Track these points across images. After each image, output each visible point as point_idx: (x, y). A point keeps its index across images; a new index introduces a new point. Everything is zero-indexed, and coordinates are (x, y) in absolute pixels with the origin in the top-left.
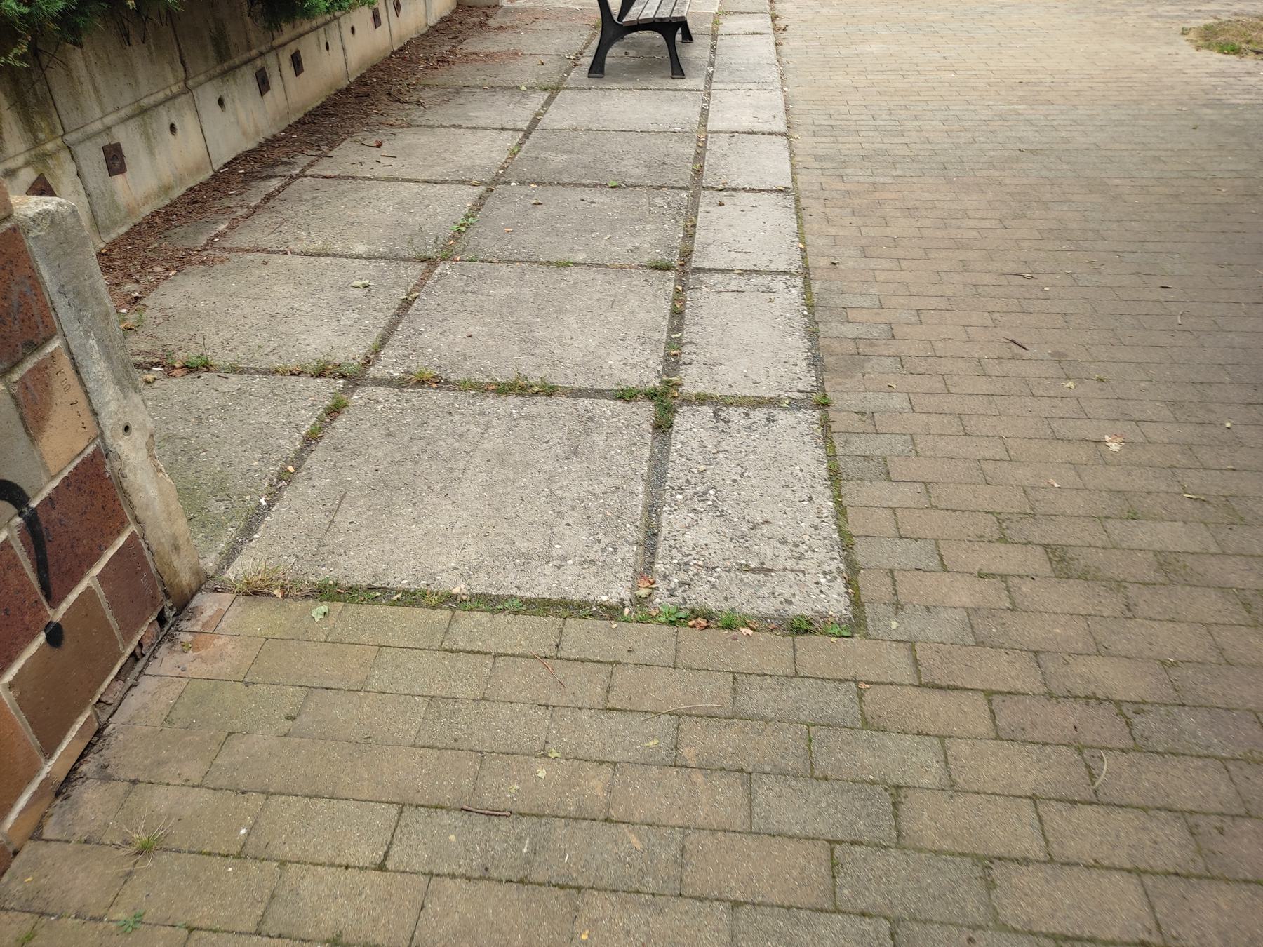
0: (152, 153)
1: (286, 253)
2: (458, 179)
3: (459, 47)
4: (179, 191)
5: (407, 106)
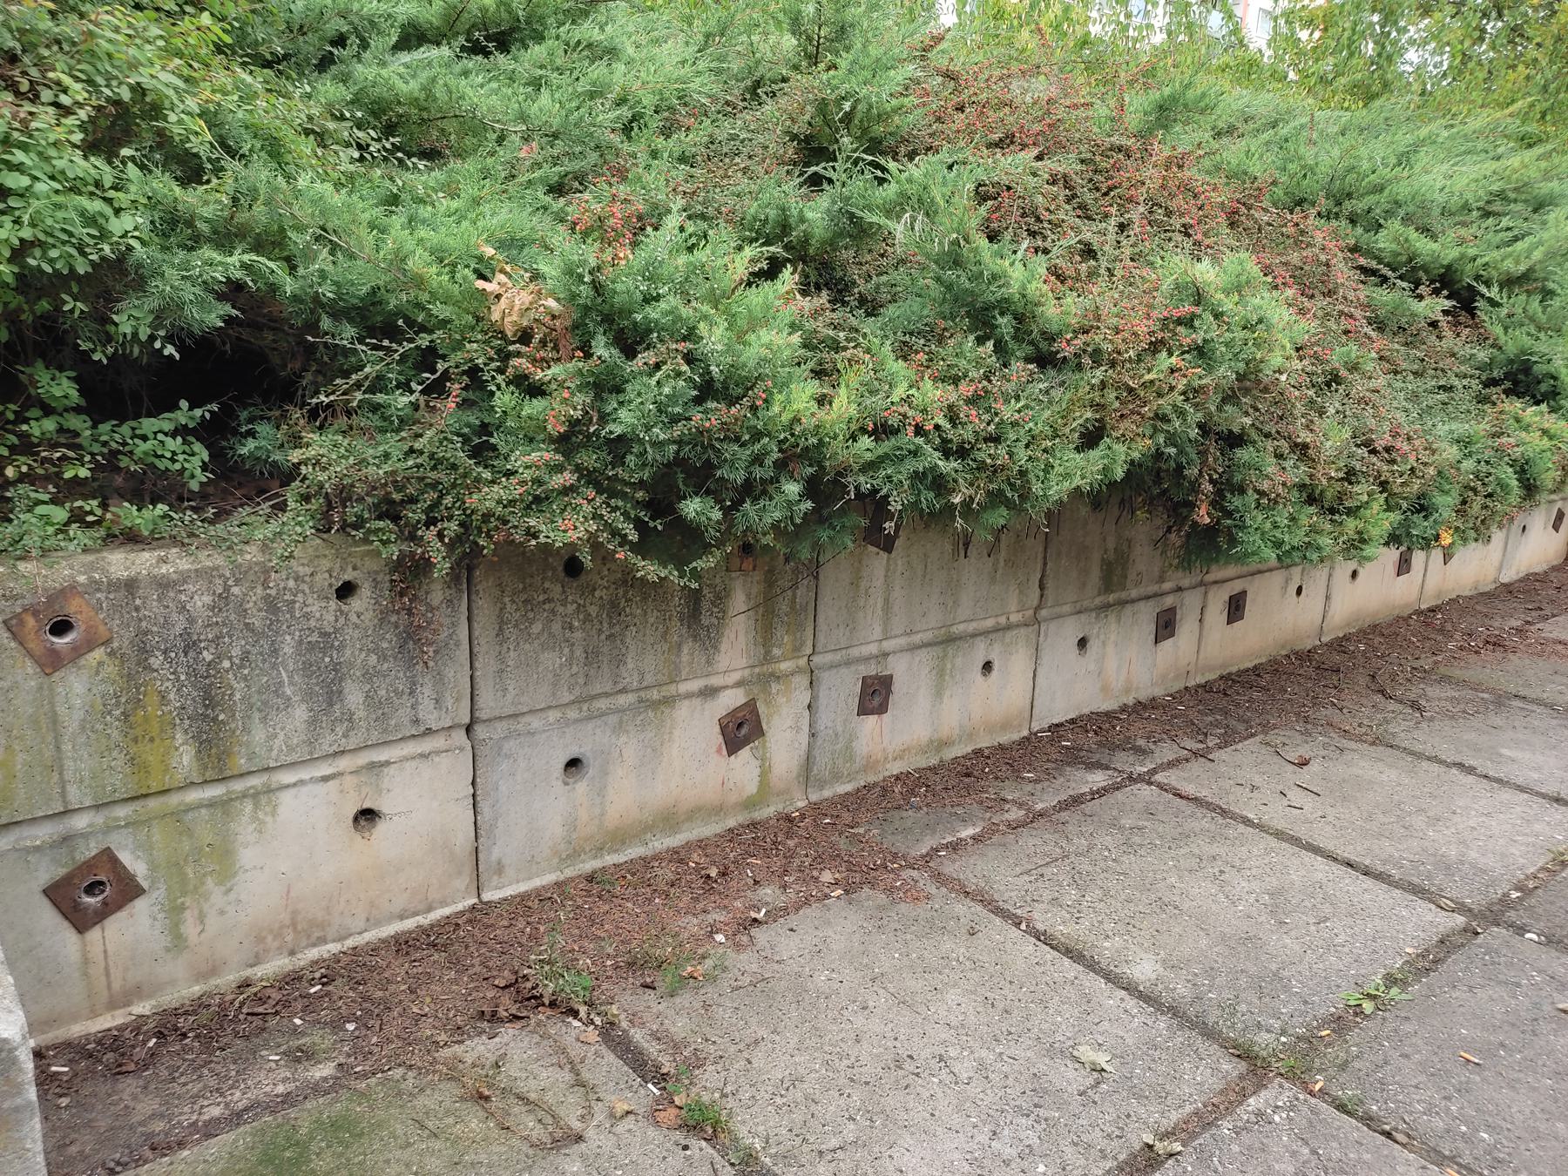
0: (938, 693)
1: (1017, 925)
2: (1416, 880)
3: (1538, 626)
4: (963, 749)
5: (1392, 706)
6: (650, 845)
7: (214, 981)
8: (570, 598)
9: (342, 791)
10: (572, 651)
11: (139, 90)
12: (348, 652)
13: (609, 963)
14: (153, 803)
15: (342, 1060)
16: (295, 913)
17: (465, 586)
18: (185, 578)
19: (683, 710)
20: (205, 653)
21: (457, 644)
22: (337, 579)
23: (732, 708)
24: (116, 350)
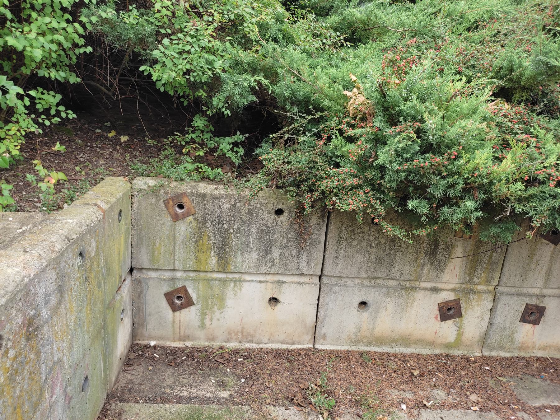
6: (394, 349)
7: (213, 343)
8: (372, 233)
9: (266, 288)
10: (370, 257)
11: (238, 15)
12: (276, 236)
13: (348, 397)
14: (202, 274)
15: (233, 393)
16: (243, 328)
17: (326, 219)
18: (222, 197)
19: (420, 295)
20: (225, 225)
21: (320, 242)
22: (276, 207)
23: (447, 300)
24: (217, 111)
